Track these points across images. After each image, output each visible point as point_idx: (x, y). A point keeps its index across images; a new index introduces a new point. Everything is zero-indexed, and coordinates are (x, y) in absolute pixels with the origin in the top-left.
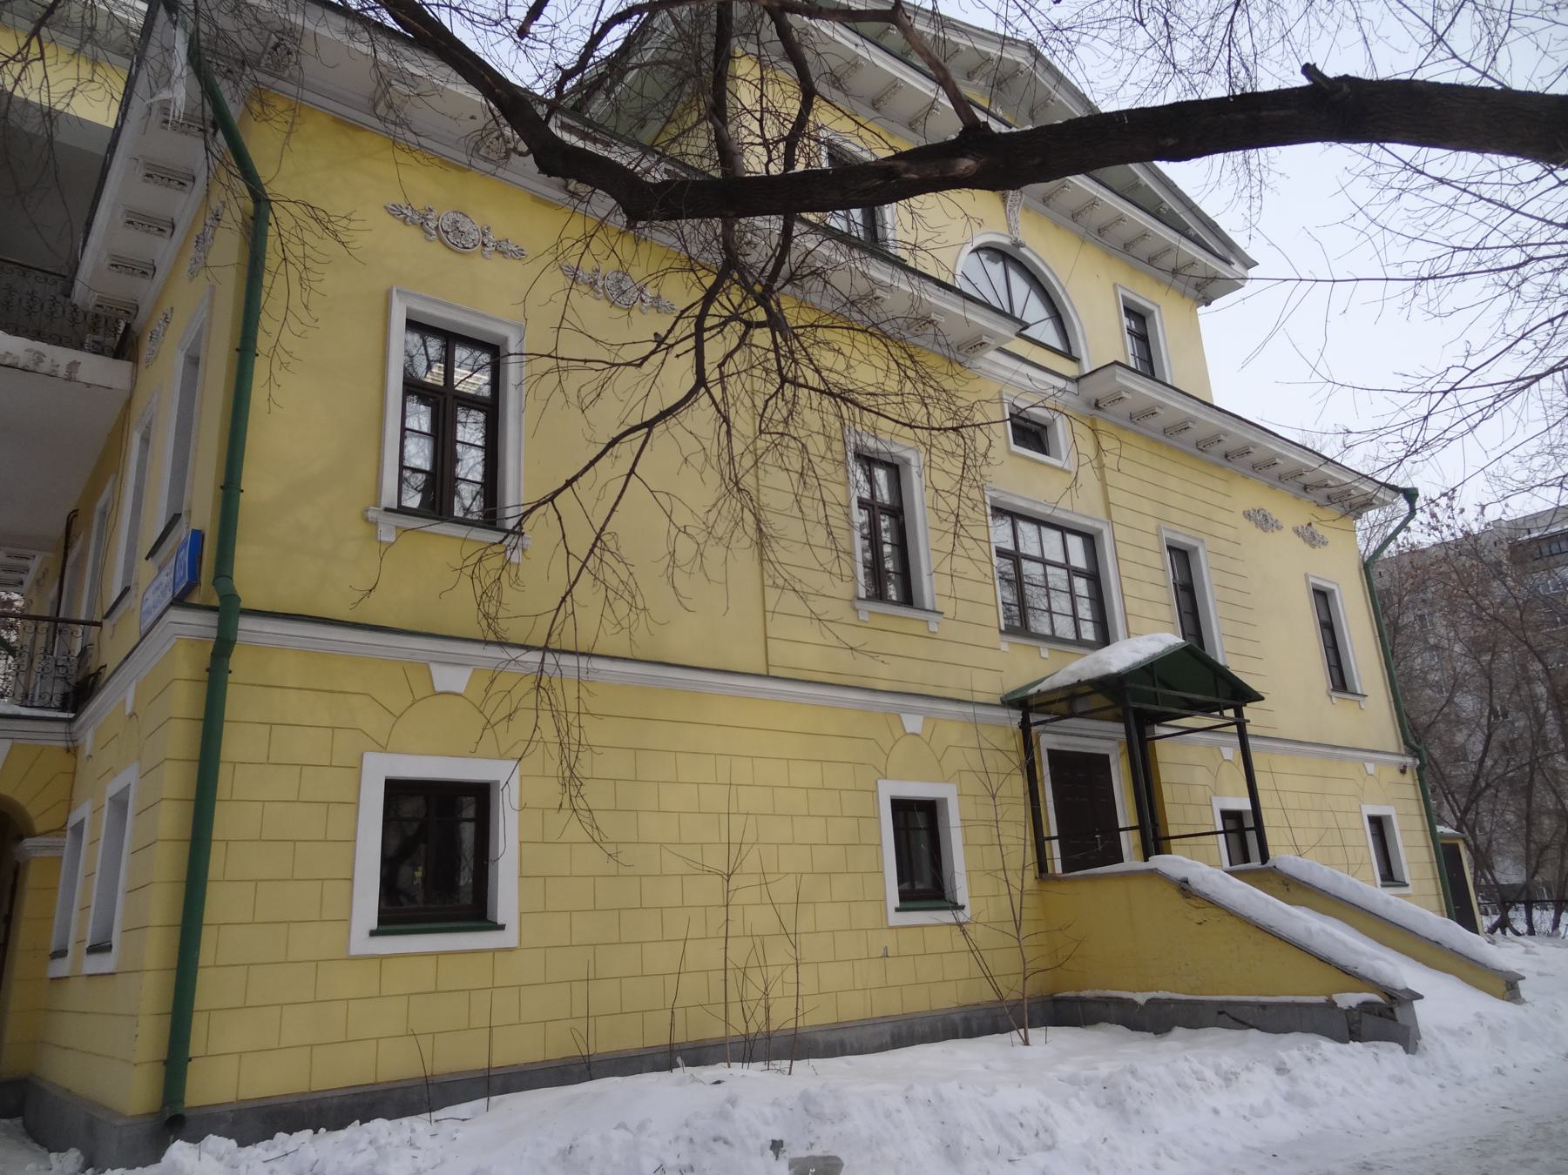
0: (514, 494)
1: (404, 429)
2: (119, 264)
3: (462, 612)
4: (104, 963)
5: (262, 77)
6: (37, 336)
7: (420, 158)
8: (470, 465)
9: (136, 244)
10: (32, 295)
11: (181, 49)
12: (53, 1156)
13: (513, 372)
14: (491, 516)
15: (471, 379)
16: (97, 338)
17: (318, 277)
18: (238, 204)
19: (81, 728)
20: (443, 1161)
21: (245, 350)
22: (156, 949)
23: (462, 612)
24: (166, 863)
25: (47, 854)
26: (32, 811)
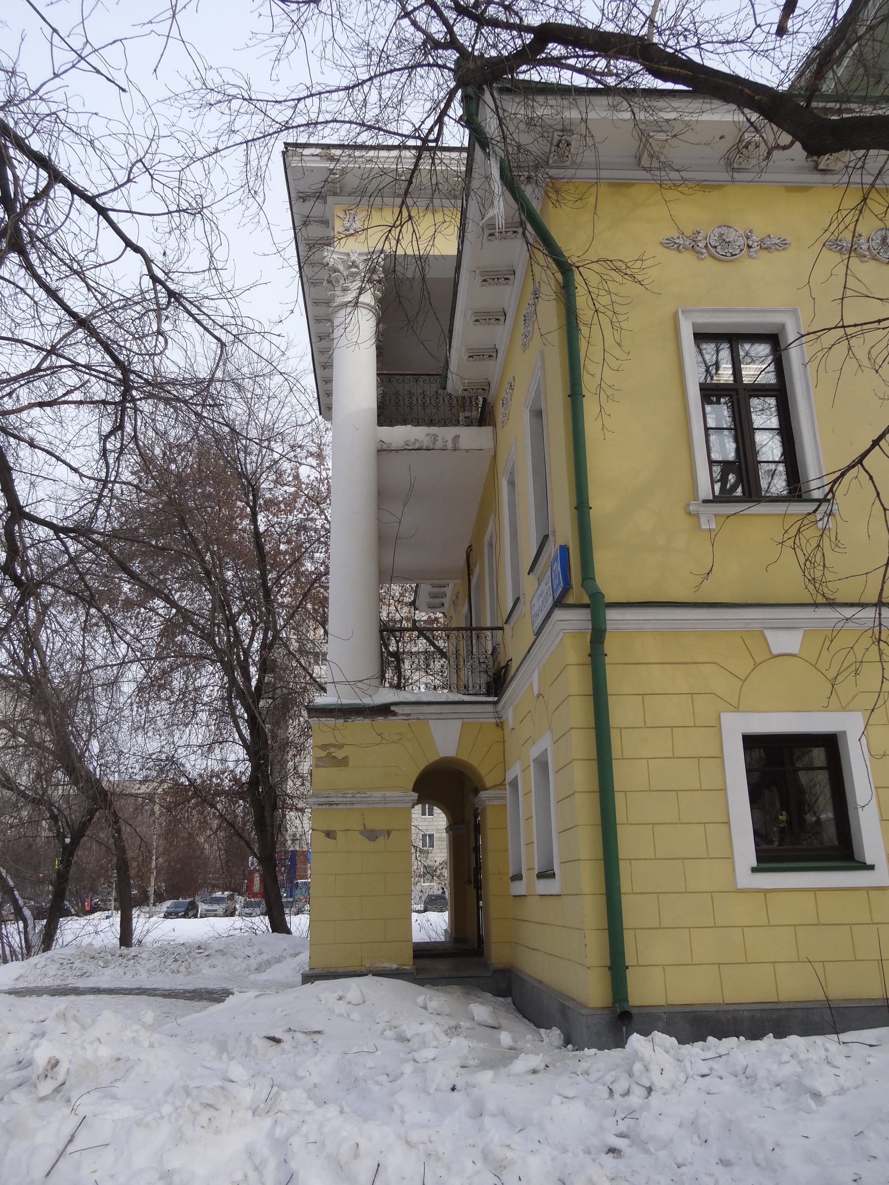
0: (816, 467)
1: (707, 429)
2: (475, 355)
3: (787, 578)
4: (544, 887)
5: (552, 172)
6: (431, 423)
7: (685, 190)
8: (769, 447)
9: (482, 335)
10: (411, 394)
11: (496, 173)
12: (542, 1031)
13: (795, 356)
14: (796, 488)
15: (756, 369)
16: (467, 414)
17: (625, 317)
18: (548, 278)
19: (503, 707)
20: (864, 1083)
21: (575, 395)
22: (588, 877)
23: (787, 578)
24: (585, 810)
25: (496, 802)
26: (483, 770)
